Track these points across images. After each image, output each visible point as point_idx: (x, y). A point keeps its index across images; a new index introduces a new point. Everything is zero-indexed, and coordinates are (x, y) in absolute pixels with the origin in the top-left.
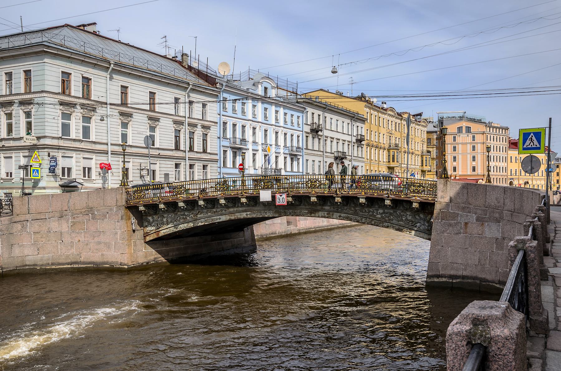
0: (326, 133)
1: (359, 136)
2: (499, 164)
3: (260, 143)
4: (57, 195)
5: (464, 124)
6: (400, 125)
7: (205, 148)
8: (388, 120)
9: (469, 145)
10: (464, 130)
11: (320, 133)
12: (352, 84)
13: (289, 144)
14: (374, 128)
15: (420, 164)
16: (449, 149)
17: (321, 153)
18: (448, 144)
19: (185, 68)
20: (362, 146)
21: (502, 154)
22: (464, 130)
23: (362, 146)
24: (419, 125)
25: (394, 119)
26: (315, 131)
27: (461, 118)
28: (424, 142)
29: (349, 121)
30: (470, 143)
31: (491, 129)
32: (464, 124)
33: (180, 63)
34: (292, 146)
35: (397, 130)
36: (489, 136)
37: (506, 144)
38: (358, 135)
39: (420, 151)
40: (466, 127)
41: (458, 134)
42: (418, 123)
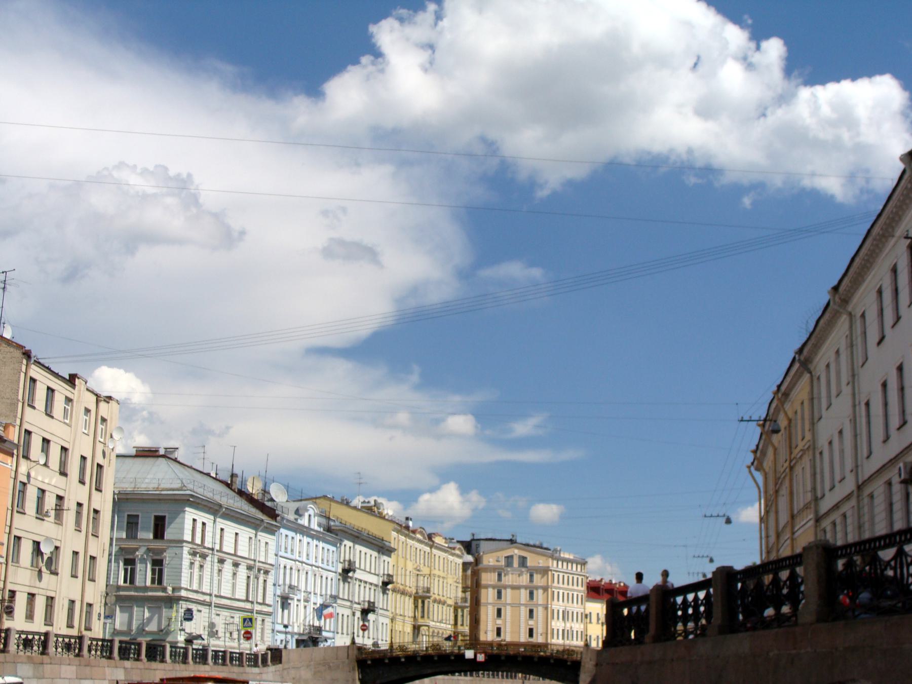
0: (358, 574)
1: (385, 577)
2: (556, 624)
3: (303, 590)
4: (252, 681)
5: (516, 552)
6: (430, 554)
7: (74, 560)
8: (416, 549)
9: (523, 591)
10: (516, 563)
11: (350, 574)
12: (360, 484)
13: (324, 593)
14: (401, 561)
15: (452, 622)
16: (488, 596)
17: (348, 604)
18: (487, 587)
19: (234, 491)
20: (349, 580)
21: (576, 608)
22: (516, 563)
23: (349, 580)
24: (413, 539)
25: (423, 546)
26: (347, 572)
27: (512, 541)
28: (458, 583)
29: (375, 554)
30: (526, 588)
31: (560, 563)
32: (516, 551)
33: (229, 486)
34: (326, 595)
35: (426, 564)
36: (556, 574)
37: (583, 589)
38: (384, 574)
39: (453, 599)
40: (520, 557)
41: (505, 569)
42: (411, 534)
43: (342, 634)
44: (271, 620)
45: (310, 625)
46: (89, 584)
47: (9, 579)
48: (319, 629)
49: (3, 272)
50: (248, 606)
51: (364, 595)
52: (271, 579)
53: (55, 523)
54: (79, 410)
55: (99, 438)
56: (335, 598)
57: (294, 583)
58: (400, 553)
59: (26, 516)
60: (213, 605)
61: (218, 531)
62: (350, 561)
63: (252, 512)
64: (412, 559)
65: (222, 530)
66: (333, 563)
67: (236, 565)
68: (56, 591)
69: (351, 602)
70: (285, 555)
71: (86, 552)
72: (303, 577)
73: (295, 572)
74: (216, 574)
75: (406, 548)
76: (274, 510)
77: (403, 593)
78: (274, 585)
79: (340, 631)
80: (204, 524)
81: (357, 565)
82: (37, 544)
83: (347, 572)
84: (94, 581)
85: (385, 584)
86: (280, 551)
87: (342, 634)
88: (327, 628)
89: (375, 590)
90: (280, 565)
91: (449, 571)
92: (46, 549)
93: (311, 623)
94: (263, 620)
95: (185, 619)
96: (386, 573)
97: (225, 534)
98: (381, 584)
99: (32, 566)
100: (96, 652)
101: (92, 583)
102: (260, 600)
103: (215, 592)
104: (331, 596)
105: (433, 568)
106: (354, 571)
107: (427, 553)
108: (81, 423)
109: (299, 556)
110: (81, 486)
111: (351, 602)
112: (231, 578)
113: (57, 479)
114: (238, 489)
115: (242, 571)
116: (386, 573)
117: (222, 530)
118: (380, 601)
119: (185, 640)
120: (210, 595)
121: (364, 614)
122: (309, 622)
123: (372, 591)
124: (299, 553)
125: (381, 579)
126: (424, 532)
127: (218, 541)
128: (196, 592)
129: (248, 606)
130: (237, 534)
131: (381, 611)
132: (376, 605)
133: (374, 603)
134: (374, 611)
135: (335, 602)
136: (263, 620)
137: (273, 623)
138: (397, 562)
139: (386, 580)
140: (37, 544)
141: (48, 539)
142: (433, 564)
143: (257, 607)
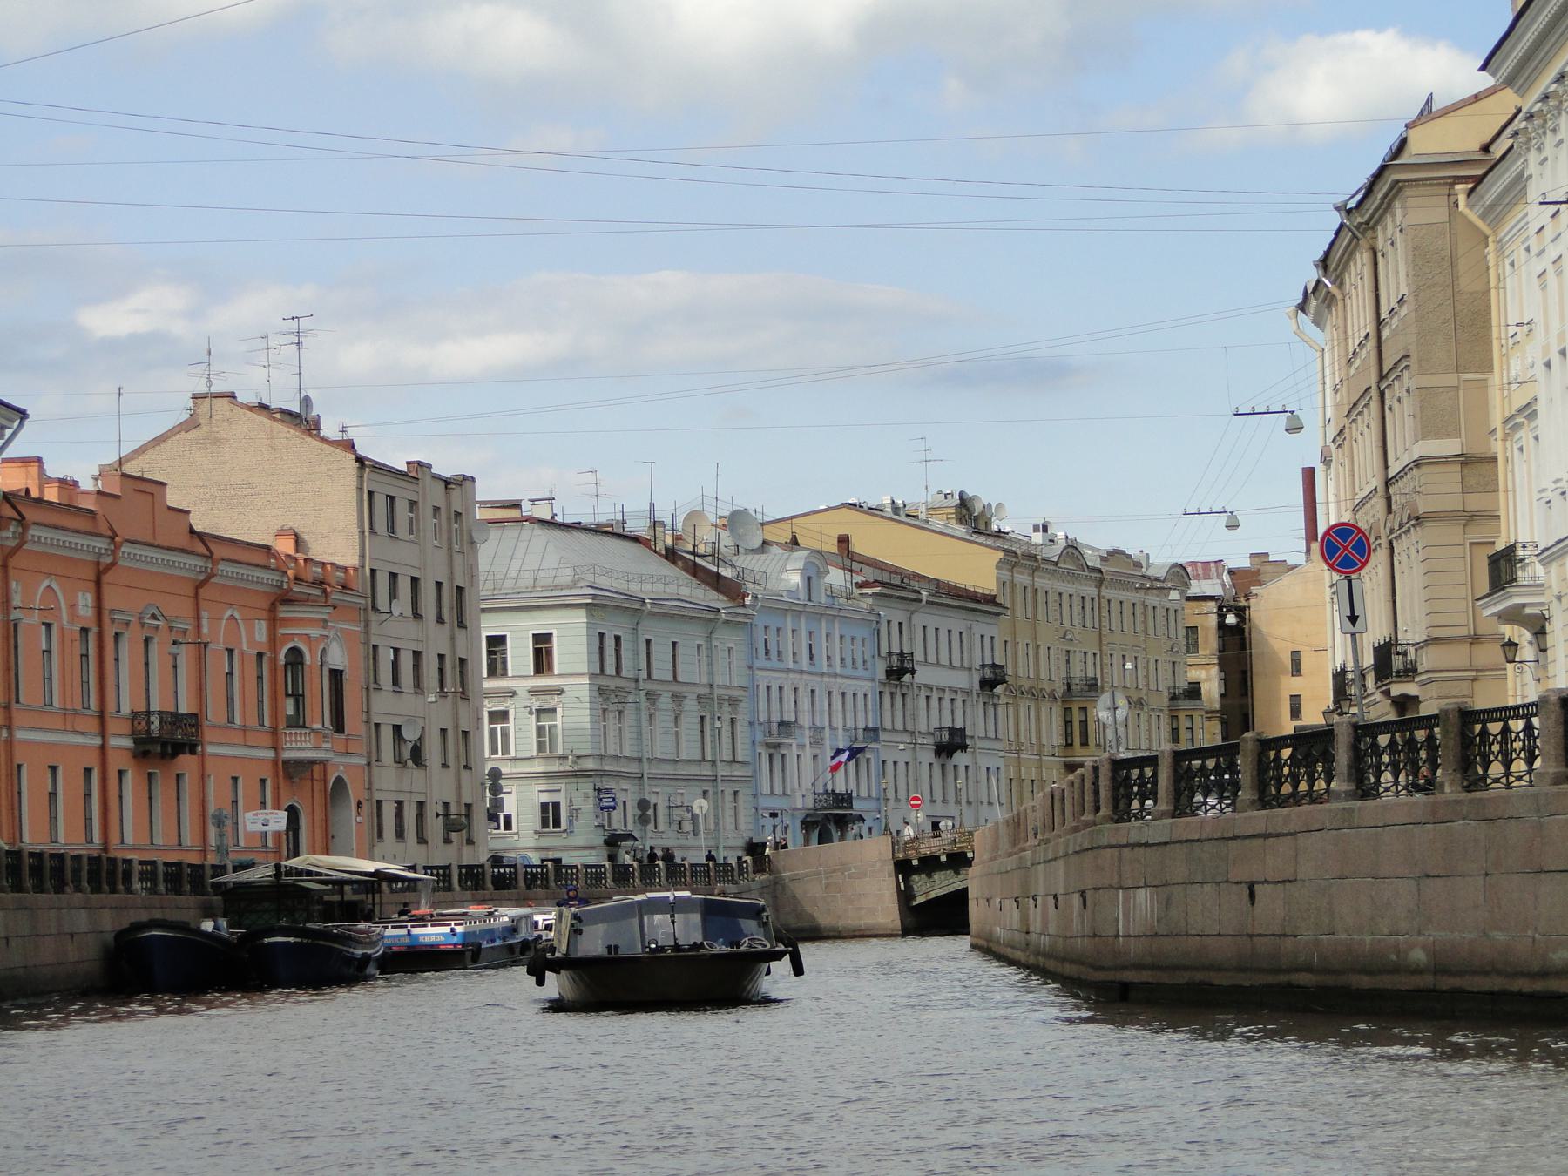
0: (924, 675)
1: (987, 671)
8: (1060, 594)
26: (899, 671)
35: (1089, 624)
38: (983, 666)
43: (897, 800)
44: (749, 791)
45: (826, 792)
46: (465, 774)
47: (375, 787)
48: (845, 799)
49: (293, 318)
50: (706, 770)
51: (933, 718)
52: (743, 717)
53: (416, 693)
54: (426, 511)
55: (456, 548)
56: (873, 732)
57: (789, 717)
58: (1019, 612)
59: (382, 692)
60: (646, 776)
61: (643, 647)
62: (901, 653)
63: (697, 598)
64: (1051, 619)
65: (648, 642)
66: (864, 662)
67: (677, 698)
68: (425, 793)
69: (912, 733)
70: (768, 664)
71: (457, 726)
72: (805, 703)
73: (788, 695)
74: (645, 723)
75: (1035, 602)
76: (739, 586)
77: (1036, 695)
78: (751, 724)
79: (891, 794)
80: (618, 639)
81: (919, 656)
82: (397, 729)
83: (899, 671)
84: (471, 769)
85: (988, 685)
86: (757, 658)
87: (897, 800)
88: (864, 793)
89: (964, 701)
90: (758, 686)
91: (1151, 631)
92: (410, 735)
93: (830, 789)
94: (736, 793)
95: (196, 715)
96: (988, 661)
97: (654, 648)
98: (977, 686)
99: (395, 762)
100: (1530, 760)
101: (468, 771)
102: (727, 756)
103: (647, 755)
104: (866, 729)
105: (1105, 631)
106: (913, 672)
107: (1088, 601)
108: (430, 534)
109: (795, 662)
110: (441, 626)
111: (912, 733)
112: (673, 725)
113: (412, 629)
114: (667, 549)
115: (690, 704)
116: (830, 789)
117: (648, 642)
118: (975, 721)
119: (605, 841)
120: (640, 760)
121: (944, 755)
122: (825, 785)
123: (959, 704)
124: (794, 654)
125: (977, 678)
126: (1077, 554)
127: (644, 665)
128: (617, 758)
129: (706, 770)
130: (674, 644)
131: (980, 744)
132: (968, 733)
133: (963, 730)
134: (964, 747)
135: (877, 740)
136: (736, 793)
137: (755, 796)
138: (1014, 635)
139: (988, 674)
140: (397, 729)
141: (411, 719)
142: (1105, 623)
143: (723, 771)
